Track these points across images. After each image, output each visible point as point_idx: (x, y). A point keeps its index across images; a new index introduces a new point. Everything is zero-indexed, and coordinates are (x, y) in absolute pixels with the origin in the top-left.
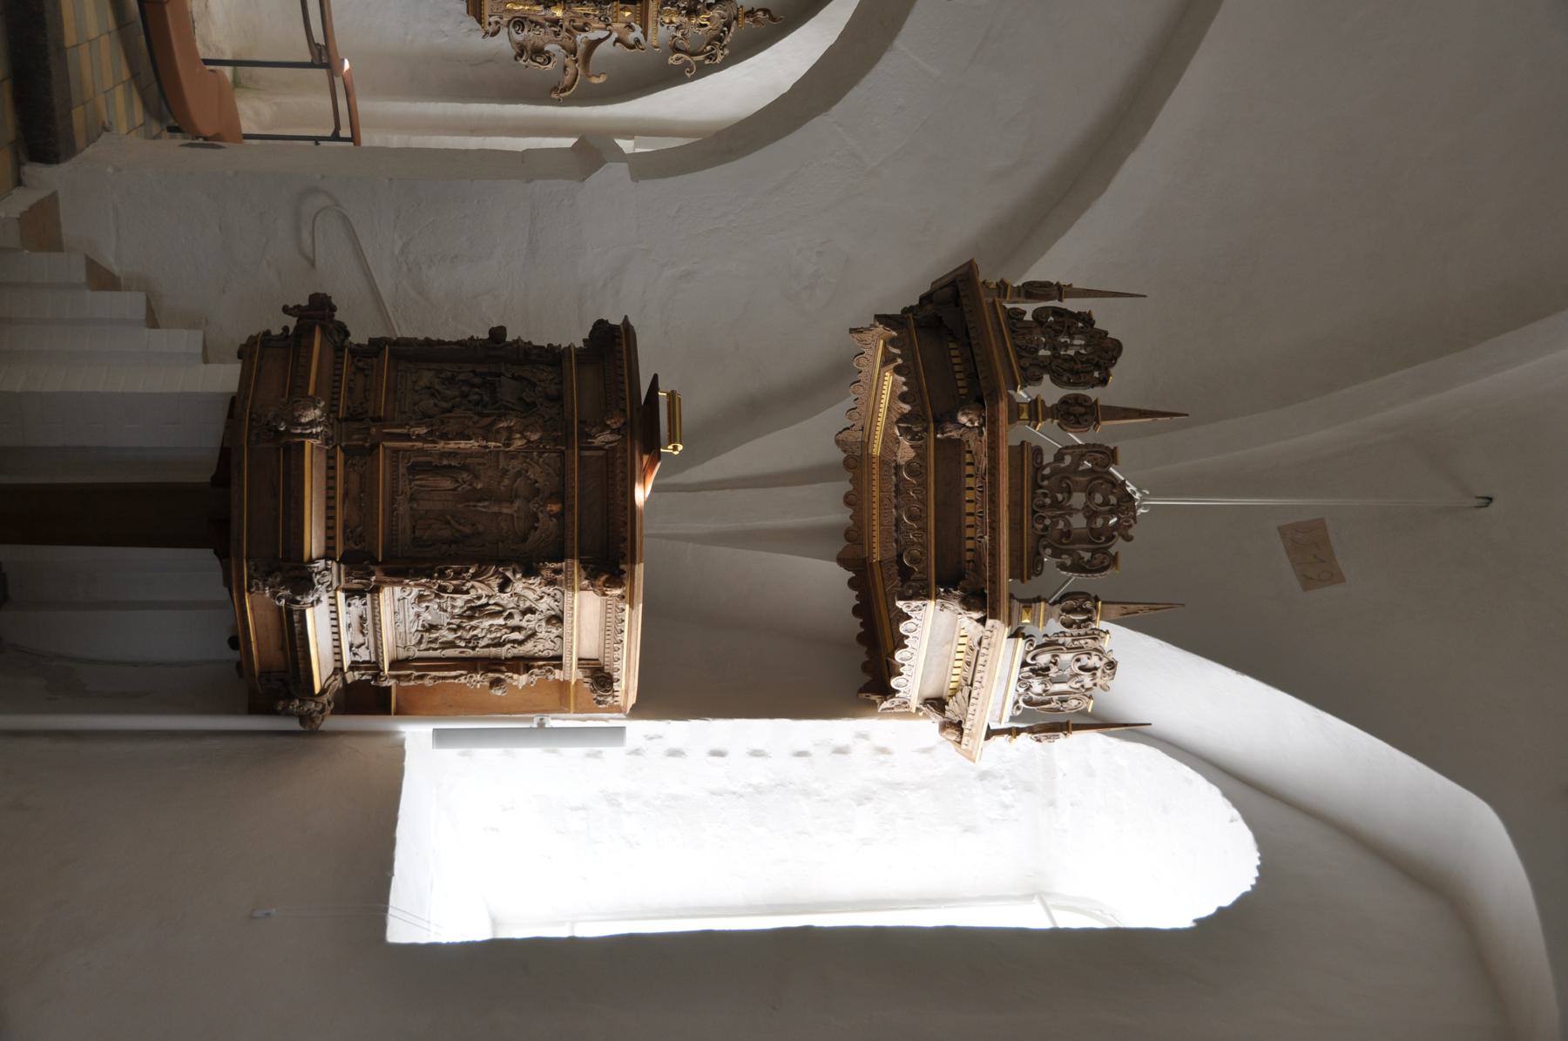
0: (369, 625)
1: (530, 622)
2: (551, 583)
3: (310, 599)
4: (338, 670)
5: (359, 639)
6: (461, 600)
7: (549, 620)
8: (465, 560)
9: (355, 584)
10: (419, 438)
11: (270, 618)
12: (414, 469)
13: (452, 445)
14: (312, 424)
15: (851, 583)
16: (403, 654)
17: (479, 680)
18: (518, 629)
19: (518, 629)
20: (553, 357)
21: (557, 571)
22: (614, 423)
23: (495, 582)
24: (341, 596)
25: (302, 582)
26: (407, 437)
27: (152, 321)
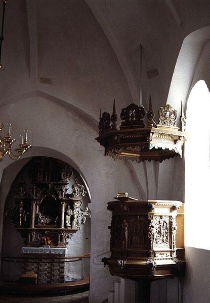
0: (162, 252)
1: (162, 222)
2: (153, 218)
3: (154, 264)
4: (172, 259)
5: (165, 255)
6: (156, 235)
7: (161, 218)
8: (148, 234)
9: (153, 255)
10: (125, 242)
11: (159, 272)
12: (131, 244)
13: (126, 236)
14: (121, 262)
15: (164, 160)
16: (169, 246)
17: (174, 232)
18: (163, 225)
19: (163, 225)
20: (114, 217)
21: (150, 217)
22: (122, 206)
23: (152, 229)
24: (155, 258)
25: (151, 264)
26: (125, 245)
27: (114, 292)
